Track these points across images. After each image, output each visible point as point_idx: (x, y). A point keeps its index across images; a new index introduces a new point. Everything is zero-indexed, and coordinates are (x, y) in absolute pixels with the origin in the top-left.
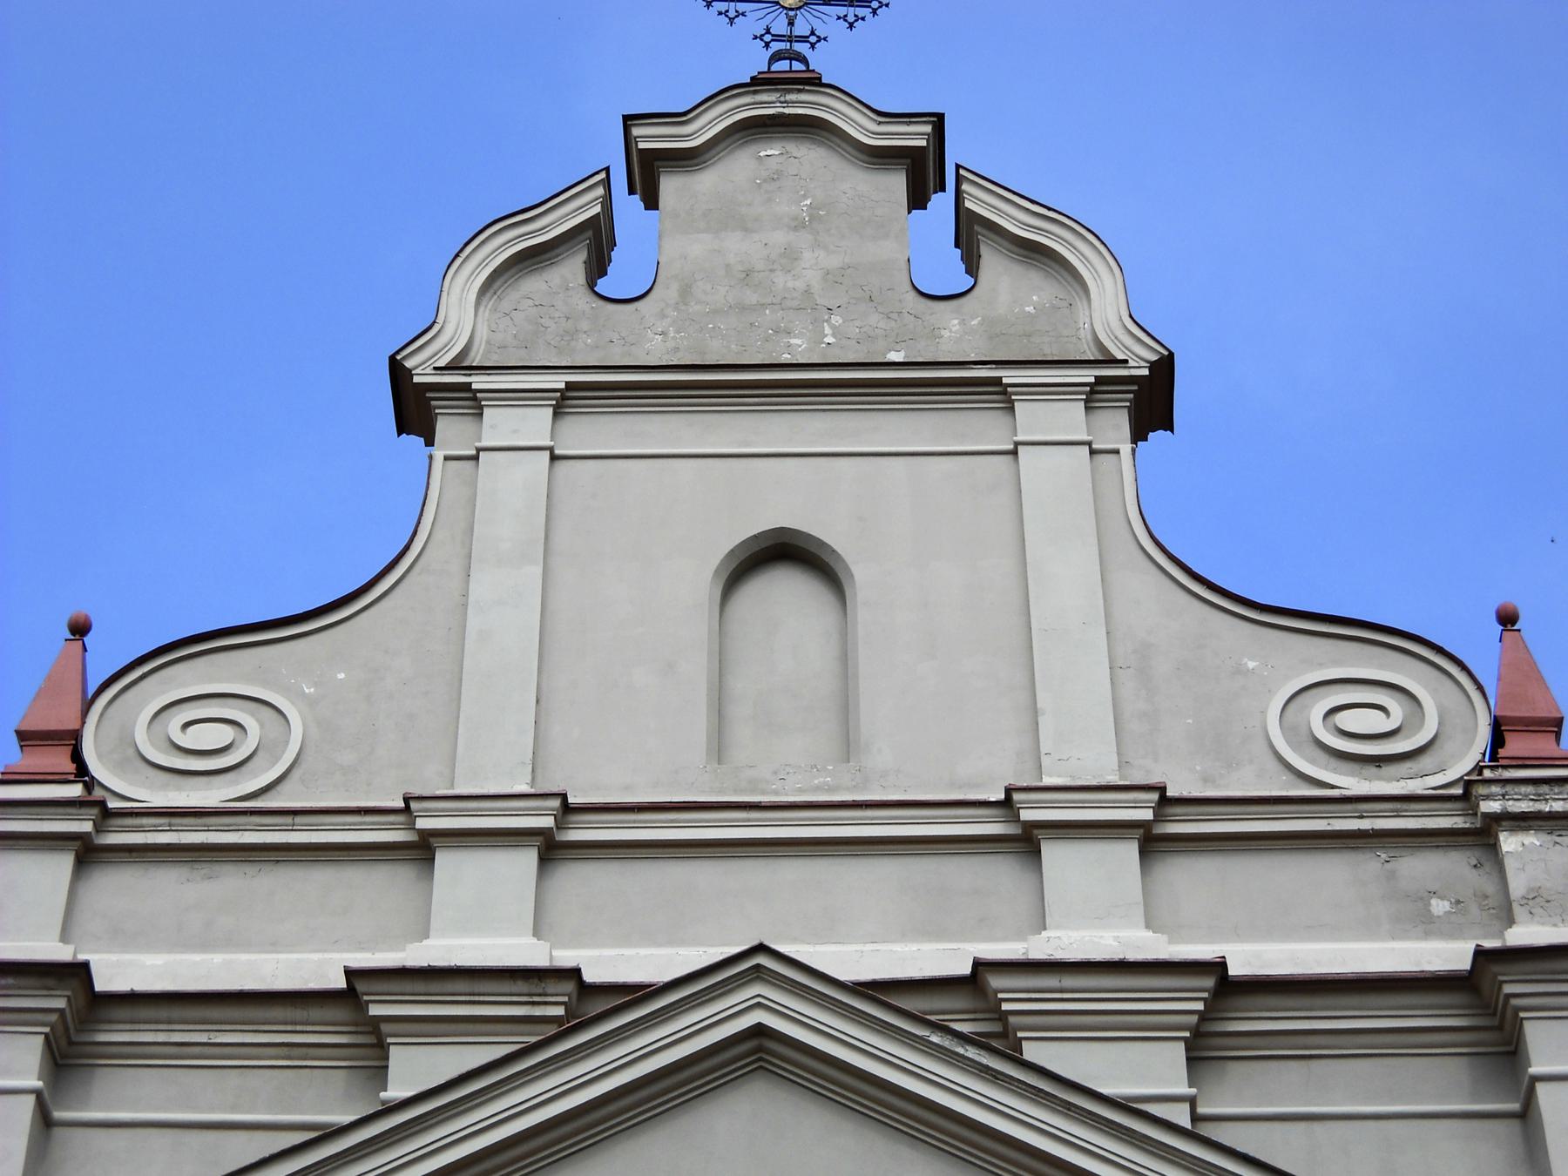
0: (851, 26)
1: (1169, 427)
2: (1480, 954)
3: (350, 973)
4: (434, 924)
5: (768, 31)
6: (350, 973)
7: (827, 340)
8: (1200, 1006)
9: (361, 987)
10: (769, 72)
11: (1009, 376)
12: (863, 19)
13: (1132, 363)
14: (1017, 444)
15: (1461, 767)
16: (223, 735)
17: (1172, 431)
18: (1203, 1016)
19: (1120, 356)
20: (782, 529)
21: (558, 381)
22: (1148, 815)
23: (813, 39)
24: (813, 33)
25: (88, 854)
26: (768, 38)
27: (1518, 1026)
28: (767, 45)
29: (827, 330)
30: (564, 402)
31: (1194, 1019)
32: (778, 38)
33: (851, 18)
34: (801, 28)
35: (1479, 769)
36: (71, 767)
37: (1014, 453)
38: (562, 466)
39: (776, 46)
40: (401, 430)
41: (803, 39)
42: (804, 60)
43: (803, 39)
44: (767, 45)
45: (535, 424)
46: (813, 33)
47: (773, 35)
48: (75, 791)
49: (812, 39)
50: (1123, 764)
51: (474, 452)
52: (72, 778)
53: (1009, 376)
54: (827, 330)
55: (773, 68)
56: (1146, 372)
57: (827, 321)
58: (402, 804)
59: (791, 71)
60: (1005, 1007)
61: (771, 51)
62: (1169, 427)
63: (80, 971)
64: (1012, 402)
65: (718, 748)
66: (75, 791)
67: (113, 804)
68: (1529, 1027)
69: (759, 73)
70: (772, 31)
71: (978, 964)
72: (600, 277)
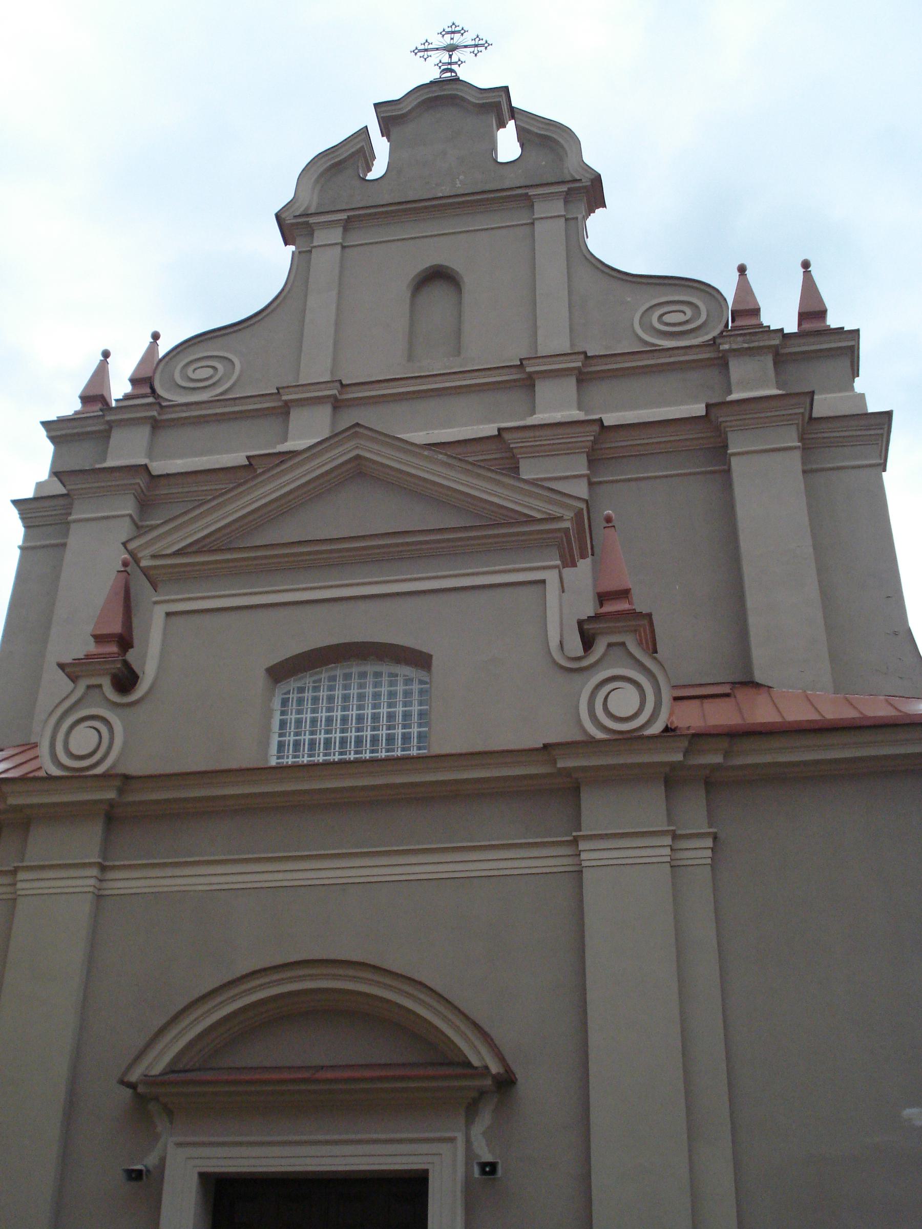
0: (476, 55)
1: (604, 206)
2: (499, 430)
3: (248, 458)
4: (290, 435)
5: (440, 62)
6: (248, 458)
7: (457, 186)
8: (592, 438)
9: (253, 462)
10: (440, 77)
11: (531, 192)
12: (481, 51)
13: (583, 181)
14: (534, 219)
15: (715, 333)
16: (209, 372)
17: (606, 207)
18: (594, 442)
19: (578, 178)
20: (441, 266)
21: (343, 216)
22: (579, 364)
23: (459, 63)
24: (459, 60)
25: (156, 425)
26: (440, 65)
27: (726, 433)
28: (440, 67)
29: (458, 182)
30: (348, 225)
31: (589, 444)
32: (444, 64)
33: (476, 52)
34: (454, 59)
35: (722, 332)
36: (148, 391)
37: (533, 224)
38: (347, 250)
39: (443, 67)
40: (286, 245)
41: (456, 63)
42: (455, 72)
43: (456, 63)
44: (440, 67)
45: (336, 235)
46: (459, 60)
47: (443, 63)
48: (151, 400)
49: (460, 63)
50: (572, 345)
51: (309, 249)
52: (149, 395)
53: (531, 192)
54: (458, 182)
55: (443, 76)
56: (589, 184)
57: (458, 178)
58: (276, 391)
59: (451, 76)
60: (512, 446)
61: (441, 69)
62: (604, 206)
63: (601, 420)
64: (533, 203)
65: (410, 358)
66: (151, 400)
67: (164, 404)
68: (730, 435)
69: (434, 79)
70: (442, 62)
71: (499, 430)
72: (368, 172)
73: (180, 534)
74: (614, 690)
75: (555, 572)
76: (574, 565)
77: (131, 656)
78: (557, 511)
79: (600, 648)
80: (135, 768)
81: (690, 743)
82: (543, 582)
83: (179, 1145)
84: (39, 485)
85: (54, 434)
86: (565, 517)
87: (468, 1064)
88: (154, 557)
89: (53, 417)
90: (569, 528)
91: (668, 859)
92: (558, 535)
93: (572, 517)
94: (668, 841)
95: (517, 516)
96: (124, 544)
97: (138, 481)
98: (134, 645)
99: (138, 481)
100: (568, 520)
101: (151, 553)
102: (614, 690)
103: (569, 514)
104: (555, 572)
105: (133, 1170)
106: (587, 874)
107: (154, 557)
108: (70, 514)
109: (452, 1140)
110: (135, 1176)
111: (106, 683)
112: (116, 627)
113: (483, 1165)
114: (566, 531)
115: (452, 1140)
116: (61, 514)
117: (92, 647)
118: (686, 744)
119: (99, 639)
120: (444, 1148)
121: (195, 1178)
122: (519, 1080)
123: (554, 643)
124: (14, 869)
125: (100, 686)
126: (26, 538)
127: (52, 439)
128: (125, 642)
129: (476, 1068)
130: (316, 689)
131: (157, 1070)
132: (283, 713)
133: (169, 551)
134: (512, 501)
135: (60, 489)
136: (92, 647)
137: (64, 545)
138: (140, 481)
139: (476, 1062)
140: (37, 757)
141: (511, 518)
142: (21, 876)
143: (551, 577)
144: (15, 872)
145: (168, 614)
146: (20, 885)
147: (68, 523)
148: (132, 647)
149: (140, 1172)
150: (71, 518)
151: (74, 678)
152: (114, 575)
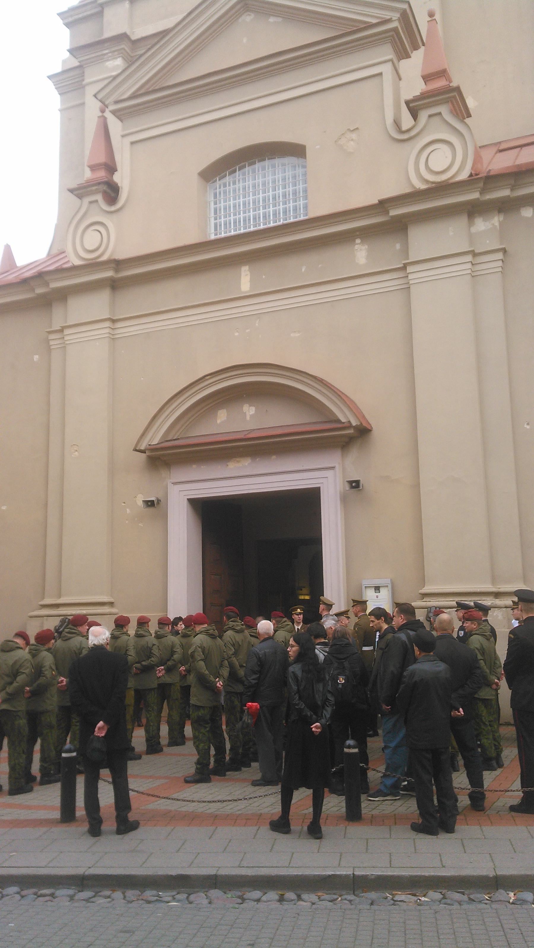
73: (130, 82)
74: (432, 151)
75: (390, 65)
76: (408, 56)
77: (117, 178)
78: (386, 15)
79: (423, 116)
80: (121, 255)
81: (485, 183)
82: (380, 74)
83: (175, 483)
84: (64, 62)
85: (67, 21)
86: (394, 19)
87: (339, 421)
88: (116, 102)
89: (65, 9)
90: (397, 27)
91: (469, 271)
92: (391, 33)
93: (399, 18)
94: (469, 258)
95: (357, 24)
96: (95, 96)
97: (123, 46)
98: (118, 169)
99: (123, 46)
100: (395, 20)
101: (113, 100)
102: (432, 151)
103: (396, 16)
104: (389, 65)
105: (149, 501)
106: (413, 289)
107: (116, 102)
108: (83, 80)
109: (333, 468)
110: (150, 504)
111: (99, 197)
112: (102, 159)
113: (351, 482)
114: (395, 30)
115: (333, 468)
116: (77, 82)
117: (88, 174)
118: (481, 185)
119: (93, 168)
120: (329, 473)
121: (186, 502)
122: (373, 428)
123: (389, 121)
124: (61, 328)
125: (96, 201)
126: (62, 102)
127: (67, 25)
128: (111, 168)
129: (344, 423)
130: (234, 183)
131: (155, 441)
132: (215, 203)
133: (125, 96)
134: (354, 13)
135: (75, 63)
136: (88, 174)
137: (83, 104)
138: (125, 46)
139: (343, 420)
140: (66, 256)
141: (354, 26)
142: (410, 269)
143: (387, 69)
144: (61, 331)
145: (132, 143)
146: (66, 338)
147: (84, 87)
148: (117, 171)
149: (152, 502)
150: (84, 83)
151: (80, 197)
152: (96, 119)
